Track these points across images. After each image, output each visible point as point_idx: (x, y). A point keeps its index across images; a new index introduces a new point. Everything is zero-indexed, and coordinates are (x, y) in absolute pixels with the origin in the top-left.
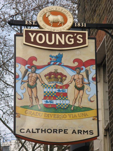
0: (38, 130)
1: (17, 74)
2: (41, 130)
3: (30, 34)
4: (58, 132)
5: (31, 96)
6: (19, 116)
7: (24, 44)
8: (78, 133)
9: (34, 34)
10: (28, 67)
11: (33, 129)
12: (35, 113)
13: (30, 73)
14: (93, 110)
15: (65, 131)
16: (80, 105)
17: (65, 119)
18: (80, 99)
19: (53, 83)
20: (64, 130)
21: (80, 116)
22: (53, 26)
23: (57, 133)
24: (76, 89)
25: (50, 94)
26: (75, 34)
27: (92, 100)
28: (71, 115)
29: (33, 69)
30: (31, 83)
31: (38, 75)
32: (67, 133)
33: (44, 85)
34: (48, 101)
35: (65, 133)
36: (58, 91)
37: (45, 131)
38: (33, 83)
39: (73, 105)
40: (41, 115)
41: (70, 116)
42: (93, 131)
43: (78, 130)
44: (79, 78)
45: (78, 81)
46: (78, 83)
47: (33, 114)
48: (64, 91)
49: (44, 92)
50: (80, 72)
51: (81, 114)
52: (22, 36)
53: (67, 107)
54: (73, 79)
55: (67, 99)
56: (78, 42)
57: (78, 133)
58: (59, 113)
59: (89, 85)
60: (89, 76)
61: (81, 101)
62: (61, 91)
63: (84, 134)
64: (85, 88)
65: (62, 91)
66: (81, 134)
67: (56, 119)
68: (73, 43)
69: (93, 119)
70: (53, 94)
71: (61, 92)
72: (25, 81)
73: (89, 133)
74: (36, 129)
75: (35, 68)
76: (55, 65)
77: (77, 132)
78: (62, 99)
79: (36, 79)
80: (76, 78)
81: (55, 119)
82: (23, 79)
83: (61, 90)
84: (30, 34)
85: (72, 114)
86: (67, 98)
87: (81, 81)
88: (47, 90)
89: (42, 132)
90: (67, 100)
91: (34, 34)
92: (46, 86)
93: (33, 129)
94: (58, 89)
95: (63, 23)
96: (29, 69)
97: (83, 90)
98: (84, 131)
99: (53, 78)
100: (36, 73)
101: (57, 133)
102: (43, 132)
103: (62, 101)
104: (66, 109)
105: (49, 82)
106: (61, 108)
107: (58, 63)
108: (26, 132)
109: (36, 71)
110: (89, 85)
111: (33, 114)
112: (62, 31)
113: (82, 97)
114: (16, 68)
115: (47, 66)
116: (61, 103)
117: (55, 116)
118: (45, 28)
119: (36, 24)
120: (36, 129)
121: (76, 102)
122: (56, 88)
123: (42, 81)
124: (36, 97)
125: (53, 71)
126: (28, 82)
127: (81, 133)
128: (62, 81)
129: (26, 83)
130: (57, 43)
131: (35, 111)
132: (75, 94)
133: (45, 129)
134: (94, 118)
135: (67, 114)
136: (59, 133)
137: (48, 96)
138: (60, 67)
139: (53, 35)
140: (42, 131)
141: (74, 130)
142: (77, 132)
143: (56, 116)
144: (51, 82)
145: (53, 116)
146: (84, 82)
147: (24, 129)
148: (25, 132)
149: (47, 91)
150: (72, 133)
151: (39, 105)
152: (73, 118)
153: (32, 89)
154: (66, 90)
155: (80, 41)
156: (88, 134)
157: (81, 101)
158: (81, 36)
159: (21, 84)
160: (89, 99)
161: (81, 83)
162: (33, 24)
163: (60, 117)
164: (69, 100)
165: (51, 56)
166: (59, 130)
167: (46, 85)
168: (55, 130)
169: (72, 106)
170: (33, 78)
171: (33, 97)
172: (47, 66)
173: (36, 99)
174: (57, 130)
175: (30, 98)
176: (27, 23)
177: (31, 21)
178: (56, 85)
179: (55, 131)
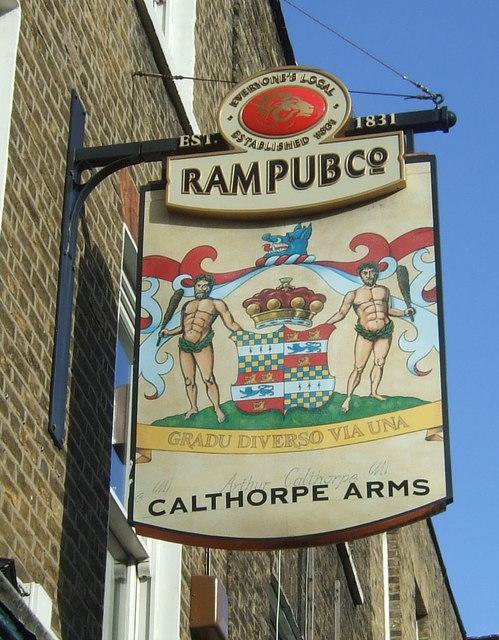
0: (213, 497)
1: (144, 315)
2: (224, 495)
4: (289, 497)
8: (369, 496)
11: (194, 498)
14: (429, 403)
18: (377, 370)
19: (274, 324)
20: (315, 488)
23: (285, 501)
24: (360, 337)
25: (261, 363)
27: (422, 368)
31: (217, 303)
32: (327, 499)
33: (240, 333)
34: (255, 388)
35: (315, 499)
36: (291, 351)
37: (240, 499)
42: (427, 482)
43: (369, 485)
44: (372, 300)
45: (368, 310)
50: (377, 276)
53: (326, 405)
55: (325, 373)
57: (369, 496)
59: (413, 320)
62: (303, 349)
63: (391, 494)
66: (381, 495)
67: (284, 449)
69: (428, 439)
70: (275, 362)
73: (411, 489)
74: (207, 496)
78: (306, 374)
83: (302, 344)
86: (327, 369)
87: (378, 308)
89: (228, 506)
92: (246, 337)
93: (194, 498)
94: (291, 345)
97: (390, 337)
98: (391, 484)
103: (305, 383)
104: (320, 409)
106: (300, 408)
107: (295, 256)
108: (172, 512)
109: (210, 292)
110: (410, 320)
115: (253, 270)
120: (207, 496)
123: (233, 321)
124: (209, 381)
126: (183, 332)
129: (177, 338)
133: (241, 493)
134: (432, 433)
135: (323, 428)
136: (295, 500)
138: (301, 268)
140: (229, 499)
141: (353, 486)
143: (283, 440)
147: (163, 501)
148: (168, 511)
150: (346, 497)
151: (220, 406)
152: (348, 441)
154: (323, 342)
156: (406, 494)
161: (381, 315)
165: (268, 238)
166: (295, 489)
167: (247, 333)
171: (199, 382)
172: (253, 270)
176: (185, 143)
178: (284, 329)
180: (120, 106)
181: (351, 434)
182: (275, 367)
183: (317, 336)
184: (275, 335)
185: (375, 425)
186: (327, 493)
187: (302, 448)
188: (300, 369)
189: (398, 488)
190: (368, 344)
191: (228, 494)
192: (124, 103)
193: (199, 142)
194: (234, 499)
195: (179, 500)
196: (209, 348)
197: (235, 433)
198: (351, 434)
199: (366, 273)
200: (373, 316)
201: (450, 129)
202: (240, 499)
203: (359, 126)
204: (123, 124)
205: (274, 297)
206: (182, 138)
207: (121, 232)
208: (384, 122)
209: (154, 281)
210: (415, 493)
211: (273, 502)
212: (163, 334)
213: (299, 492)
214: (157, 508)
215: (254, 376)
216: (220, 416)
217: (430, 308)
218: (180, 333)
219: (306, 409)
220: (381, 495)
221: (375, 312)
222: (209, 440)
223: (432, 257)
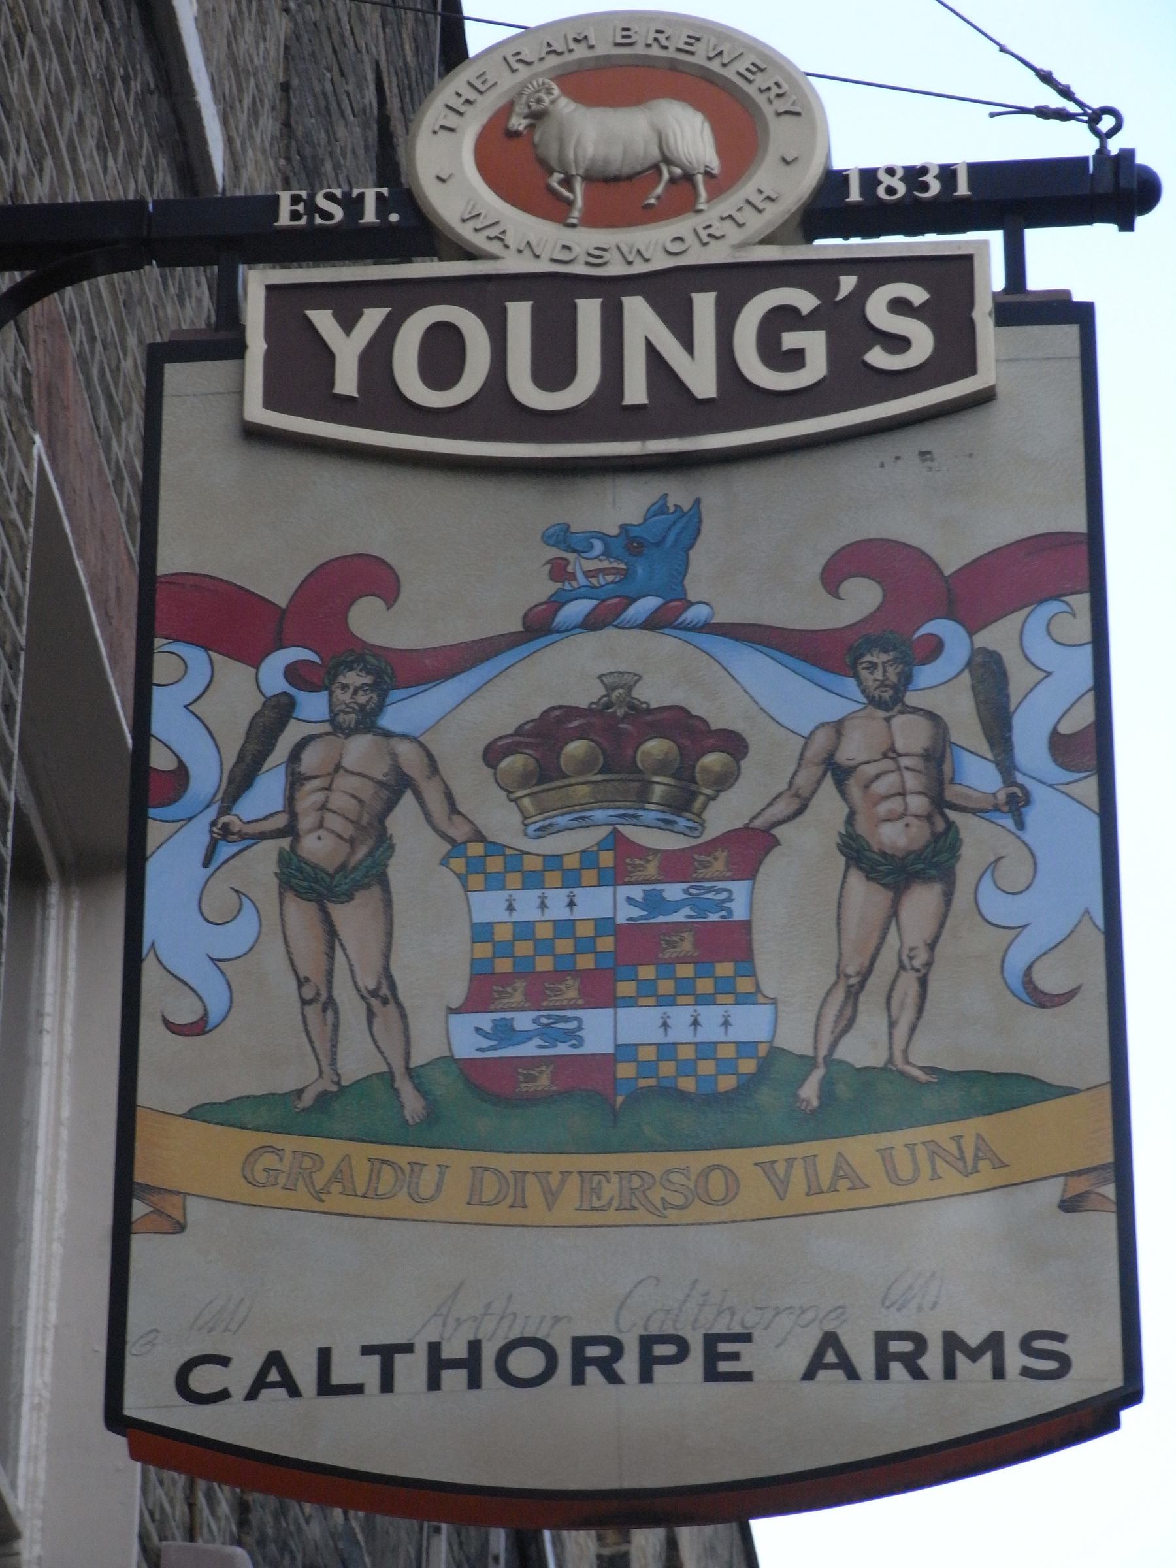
0: (387, 1354)
1: (160, 760)
2: (421, 1354)
3: (323, 320)
4: (628, 1366)
5: (318, 979)
6: (177, 1214)
7: (255, 434)
8: (882, 1374)
9: (372, 319)
10: (293, 673)
11: (324, 1355)
12: (361, 1170)
13: (312, 738)
14: (1070, 1091)
15: (723, 1347)
16: (905, 1052)
17: (724, 1213)
18: (908, 985)
19: (584, 823)
20: (711, 1341)
21: (905, 1172)
22: (592, 219)
23: (613, 1378)
24: (856, 879)
25: (544, 947)
26: (848, 284)
27: (1050, 981)
28: (798, 1172)
29: (344, 687)
30: (328, 841)
31: (405, 750)
32: (746, 1376)
33: (476, 849)
34: (524, 1021)
35: (712, 1375)
36: (636, 912)
37: (471, 1364)
38: (352, 842)
39: (823, 1052)
40: (427, 1188)
41: (786, 1182)
42: (1061, 1338)
43: (882, 1339)
44: (891, 753)
45: (880, 787)
46: (884, 808)
47: (336, 1188)
48: (719, 905)
49: (474, 926)
50: (906, 679)
51: (922, 1153)
52: (236, 349)
53: (748, 1085)
54: (818, 771)
55: (744, 985)
56: (877, 357)
57: (882, 1374)
58: (652, 1147)
59: (1021, 825)
60: (1017, 722)
61: (920, 1009)
62: (677, 906)
63: (950, 1372)
64: (968, 852)
65: (686, 911)
66: (918, 1374)
67: (612, 1216)
68: (815, 369)
69: (1070, 1205)
70: (585, 945)
71: (679, 917)
72: (250, 829)
73: (1015, 1359)
74: (367, 1350)
75: (368, 679)
76: (610, 632)
77: (864, 1360)
78: (685, 989)
79: (384, 794)
80: (851, 750)
81: (596, 1218)
82: (225, 810)
83: (674, 891)
84: (323, 320)
85: (810, 1160)
86: (753, 974)
87: (912, 782)
88: (511, 908)
89: (434, 1383)
90: (743, 1000)
91: (372, 319)
92: (495, 864)
93: (324, 1355)
94: (637, 892)
95: (708, 174)
96: (301, 696)
97: (948, 879)
98: (952, 1342)
99: (585, 766)
100: (387, 734)
101: (613, 1378)
102: (454, 1379)
103: (681, 1015)
104: (727, 1099)
105: (539, 821)
106: (669, 1093)
107: (646, 605)
108: (252, 1395)
109: (380, 708)
110: (1009, 822)
111: (336, 1177)
112: (696, 256)
113: (929, 964)
114: (157, 694)
115: (511, 641)
116: (672, 1037)
117: (597, 1191)
118: (494, 248)
119: (394, 218)
120: (367, 1350)
121: (731, 1171)
122: (617, 877)
123: (453, 809)
124: (374, 993)
125: (586, 695)
126: (290, 830)
127: (608, 1369)
128: (694, 795)
129: (269, 851)
130: (636, 391)
131: (361, 1153)
132: (851, 932)
133: (475, 1347)
134: (1080, 1185)
135: (739, 1159)
136: (646, 1377)
137: (524, 972)
138: (665, 644)
139: (589, 312)
140: (437, 1364)
141: (830, 1340)
142: (864, 1360)
143: (610, 1189)
144: (562, 821)
145: (573, 1185)
146: (951, 793)
147: (224, 1361)
148: (239, 1390)
149: (505, 916)
150: (809, 1375)
151: (410, 1072)
152: (817, 1203)
153: (340, 913)
154: (740, 889)
155: (898, 344)
156: (999, 1373)
157: (920, 1009)
158: (917, 295)
159: (207, 863)
160: (1016, 982)
161: (918, 804)
162: (361, 215)
163: (656, 1195)
164: (774, 1002)
165: (561, 537)
166: (647, 1342)
167: (498, 849)
168: (592, 1351)
169: (809, 1062)
170: (344, 782)
171: (344, 993)
172: (511, 641)
173: (371, 1015)
174: (617, 1347)
175: (305, 1002)
176: (295, 215)
177: (338, 193)
178: (617, 841)
179: (899, 1357)
180: (32, 57)
181: (825, 1181)
182: (586, 962)
183: (719, 866)
184: (588, 857)
185: (903, 1162)
186: (749, 1358)
187: (673, 1215)
188: (666, 967)
189: (974, 1355)
190: (880, 897)
191: (434, 1349)
192: (42, 42)
193: (338, 213)
194: (454, 1364)
195: (275, 1359)
196: (376, 891)
197: (461, 1161)
198: (825, 1181)
199: (873, 666)
200: (895, 805)
201: (1140, 221)
202: (471, 1364)
203: (855, 195)
204: (38, 113)
205: (580, 734)
206: (285, 197)
207: (27, 465)
208: (935, 188)
209: (195, 656)
210: (1027, 1372)
211: (578, 1378)
212: (226, 826)
213: (660, 1350)
214: (204, 1380)
215: (520, 985)
216: (413, 1104)
217: (1076, 790)
218: (278, 834)
219: (683, 1096)
220: (918, 1374)
221: (903, 794)
222: (374, 1176)
223: (1082, 627)
